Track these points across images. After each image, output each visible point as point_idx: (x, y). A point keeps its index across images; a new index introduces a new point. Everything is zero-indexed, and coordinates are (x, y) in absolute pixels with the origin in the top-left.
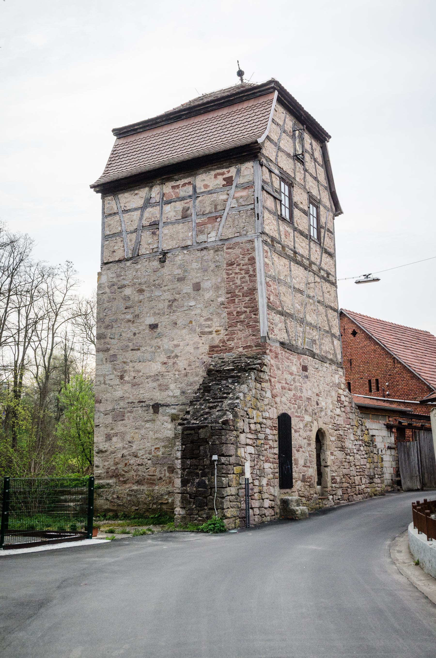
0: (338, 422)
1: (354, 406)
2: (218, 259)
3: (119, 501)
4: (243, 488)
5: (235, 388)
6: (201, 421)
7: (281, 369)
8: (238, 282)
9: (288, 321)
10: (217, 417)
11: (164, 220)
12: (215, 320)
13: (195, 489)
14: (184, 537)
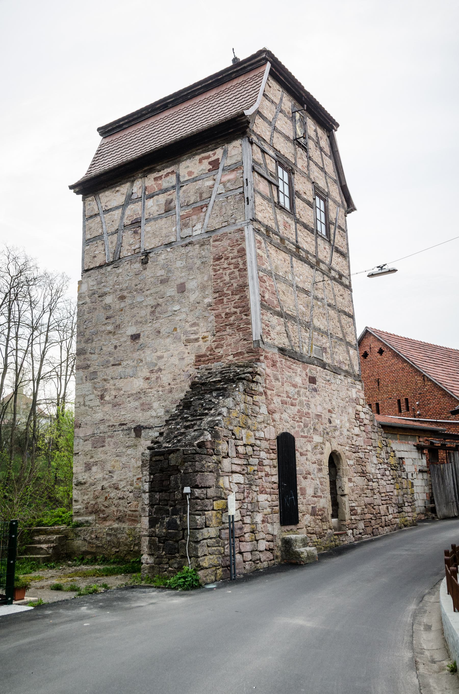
0: (357, 444)
1: (376, 424)
2: (204, 254)
3: (98, 542)
4: (227, 528)
5: (219, 403)
6: (174, 444)
7: (280, 380)
8: (227, 278)
9: (289, 324)
10: (192, 439)
11: (146, 216)
12: (202, 324)
13: (164, 531)
14: (139, 598)
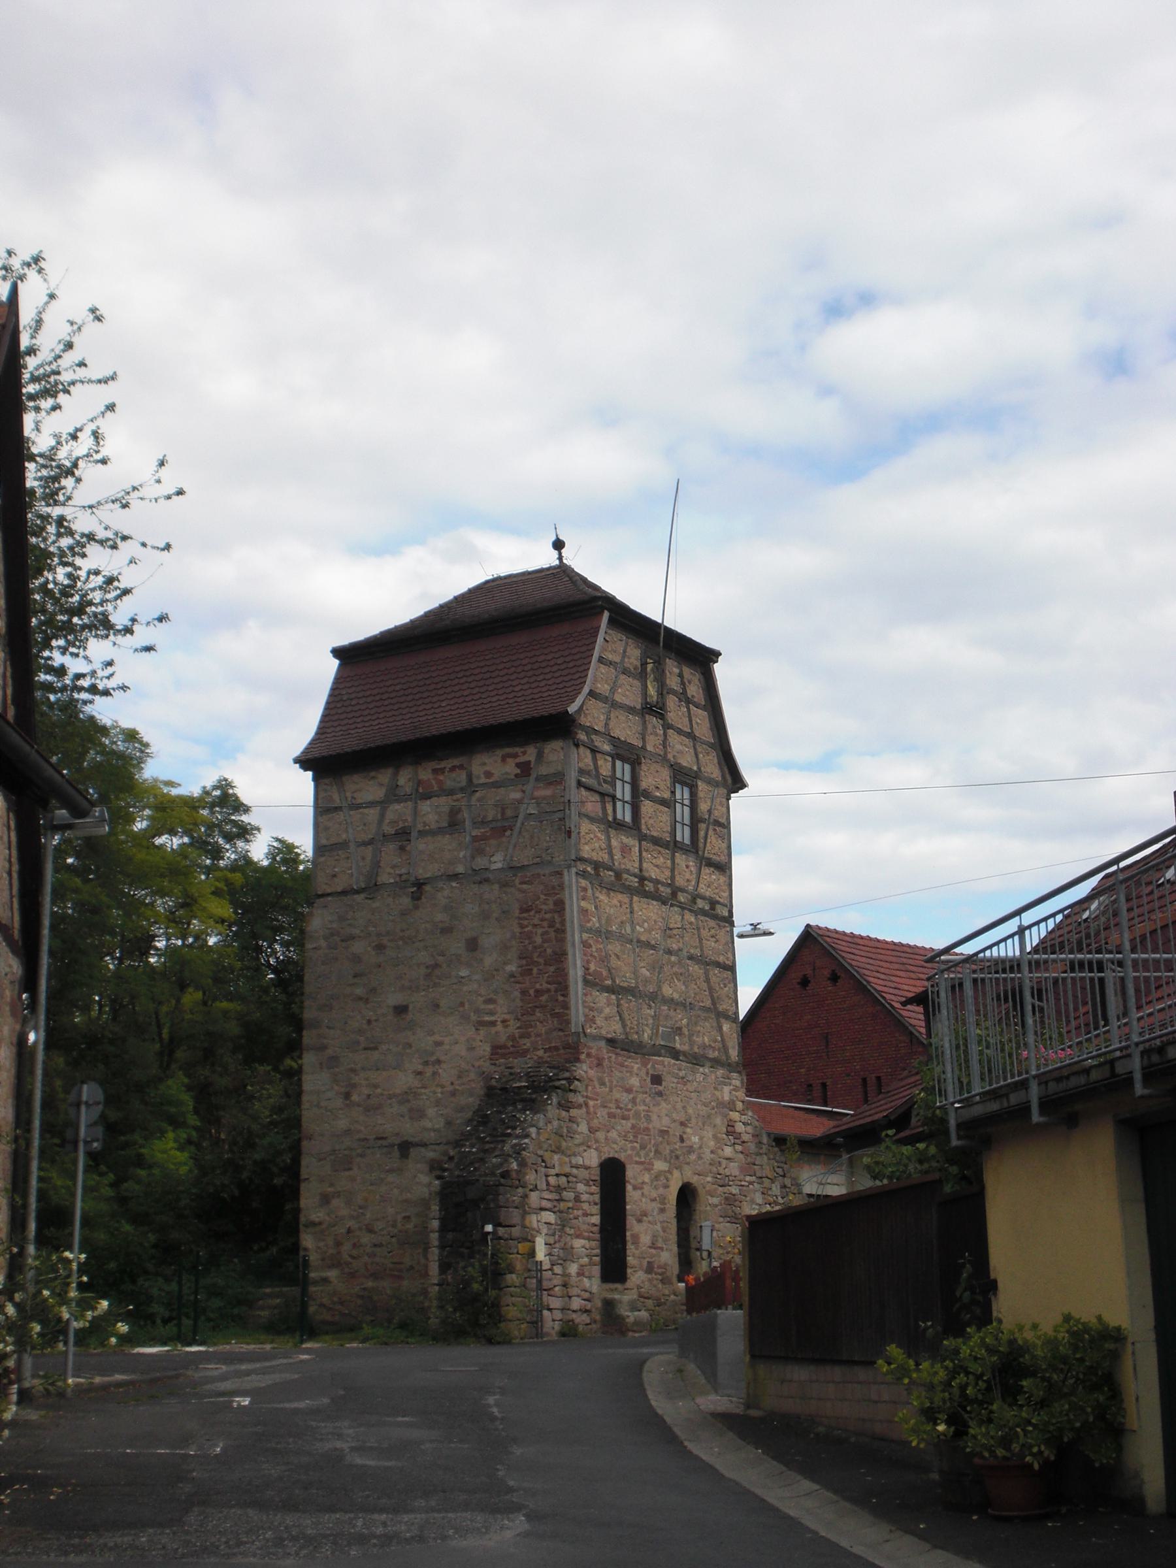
8: (538, 940)
11: (420, 827)
